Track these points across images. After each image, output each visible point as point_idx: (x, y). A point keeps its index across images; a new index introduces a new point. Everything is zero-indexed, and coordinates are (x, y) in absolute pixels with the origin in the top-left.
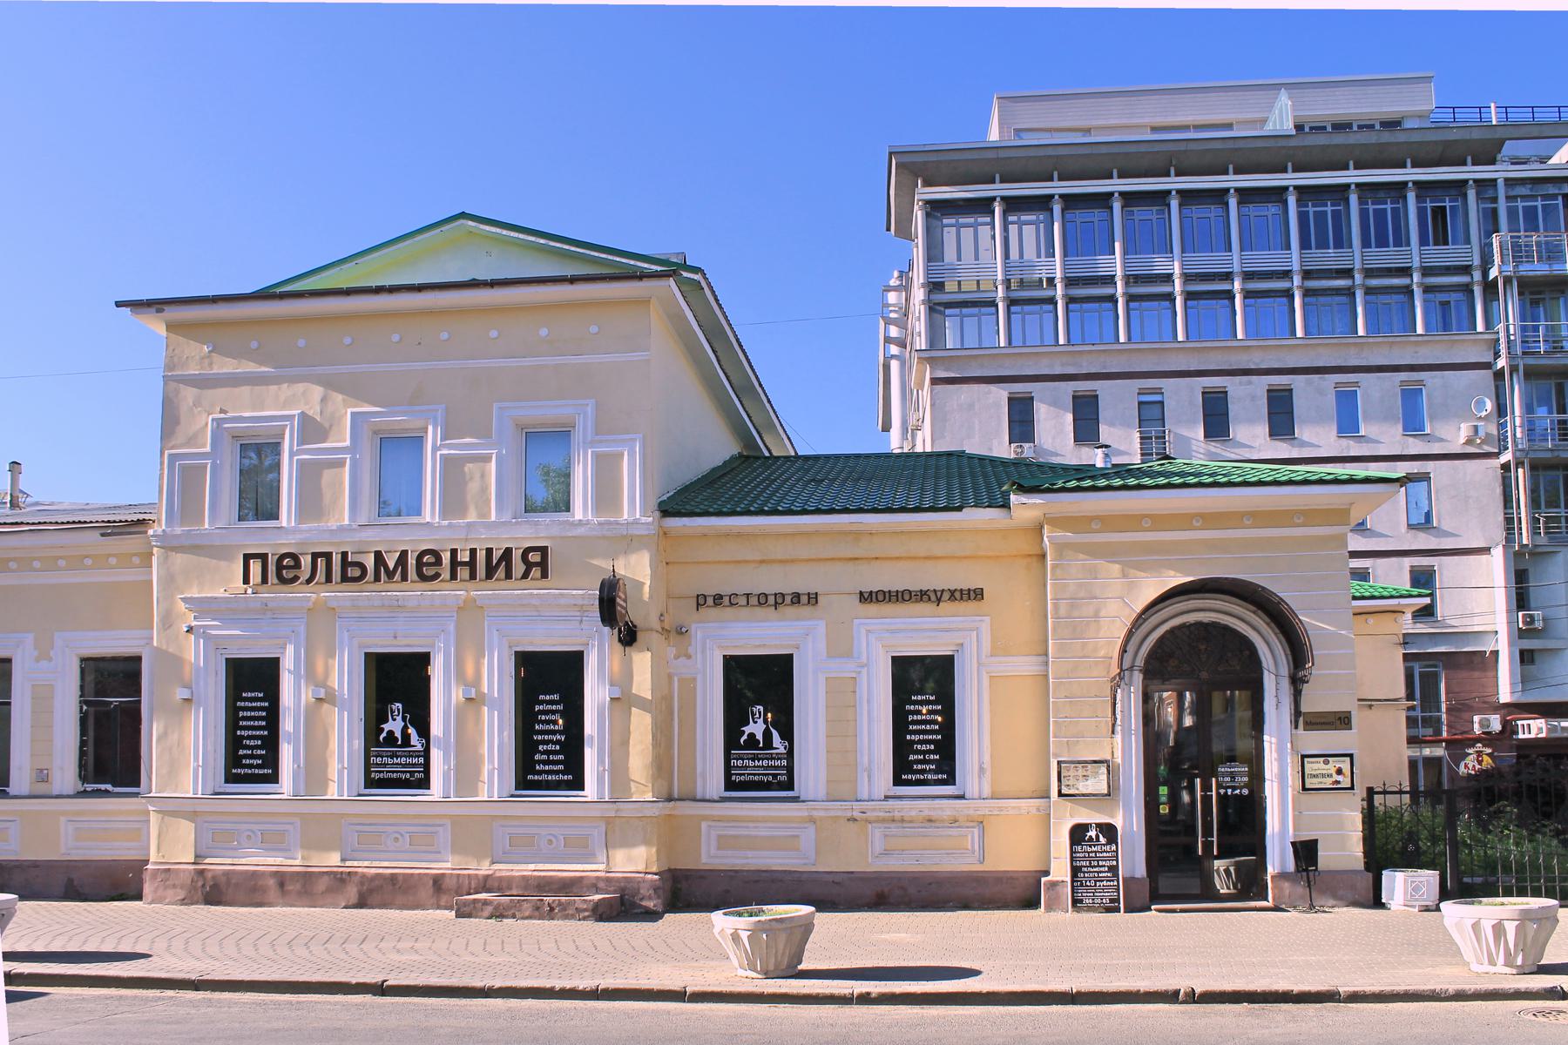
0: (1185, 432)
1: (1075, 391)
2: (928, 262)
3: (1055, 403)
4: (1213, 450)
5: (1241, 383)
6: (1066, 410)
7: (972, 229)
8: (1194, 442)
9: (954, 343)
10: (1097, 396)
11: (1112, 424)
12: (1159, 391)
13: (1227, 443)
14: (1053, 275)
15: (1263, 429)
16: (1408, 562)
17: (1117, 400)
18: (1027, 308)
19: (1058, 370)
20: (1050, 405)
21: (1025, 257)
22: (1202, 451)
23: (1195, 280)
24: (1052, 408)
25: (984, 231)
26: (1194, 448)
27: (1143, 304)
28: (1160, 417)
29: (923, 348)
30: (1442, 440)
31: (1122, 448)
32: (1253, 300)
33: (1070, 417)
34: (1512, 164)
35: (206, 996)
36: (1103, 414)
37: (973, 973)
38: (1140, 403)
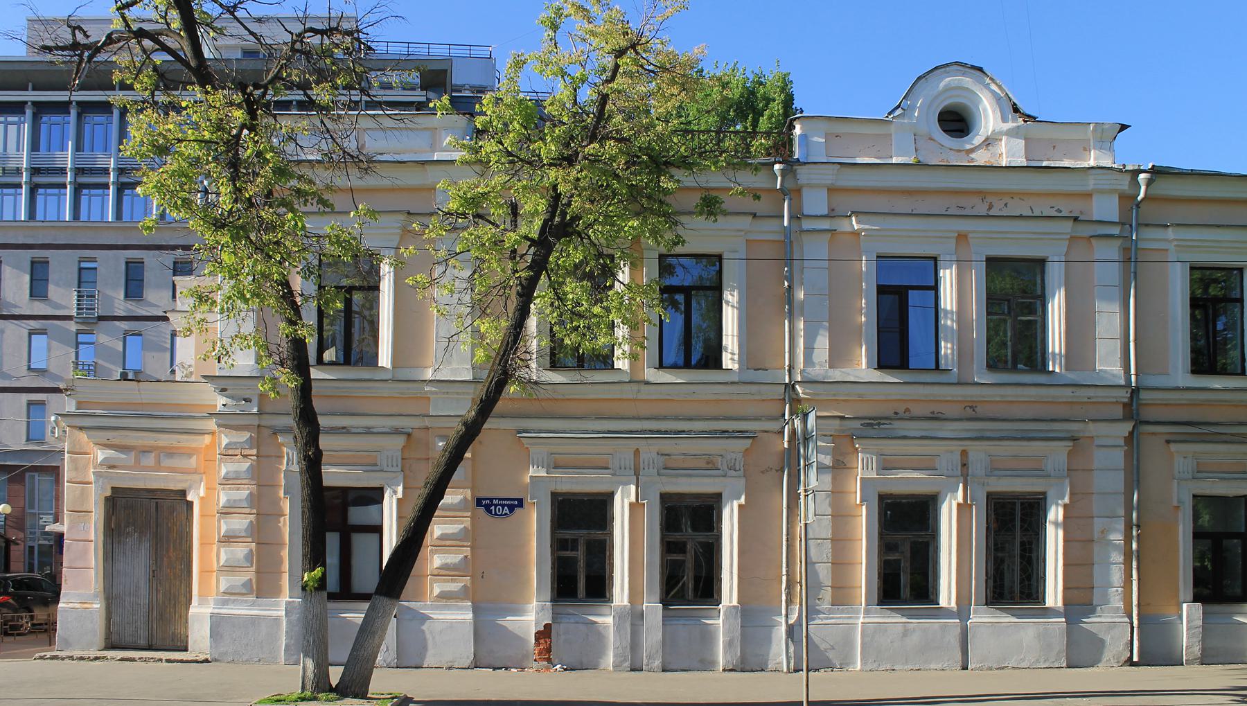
0: (109, 292)
1: (32, 258)
2: (77, 151)
3: (17, 266)
4: (130, 307)
5: (154, 256)
6: (25, 272)
7: (3, 125)
8: (116, 301)
9: (112, 219)
10: (48, 262)
11: (57, 285)
12: (93, 260)
13: (141, 302)
14: (108, 166)
15: (121, 294)
16: (25, 397)
17: (62, 265)
18: (93, 191)
19: (21, 240)
20: (13, 268)
21: (8, 151)
22: (122, 308)
23: (101, 173)
24: (15, 270)
25: (18, 124)
26: (116, 305)
27: (48, 190)
28: (34, 282)
29: (23, 219)
30: (19, 307)
31: (63, 303)
32: (130, 191)
33: (27, 278)
34: (404, 89)
35: (87, 652)
36: (53, 276)
37: (122, 659)
38: (80, 269)
